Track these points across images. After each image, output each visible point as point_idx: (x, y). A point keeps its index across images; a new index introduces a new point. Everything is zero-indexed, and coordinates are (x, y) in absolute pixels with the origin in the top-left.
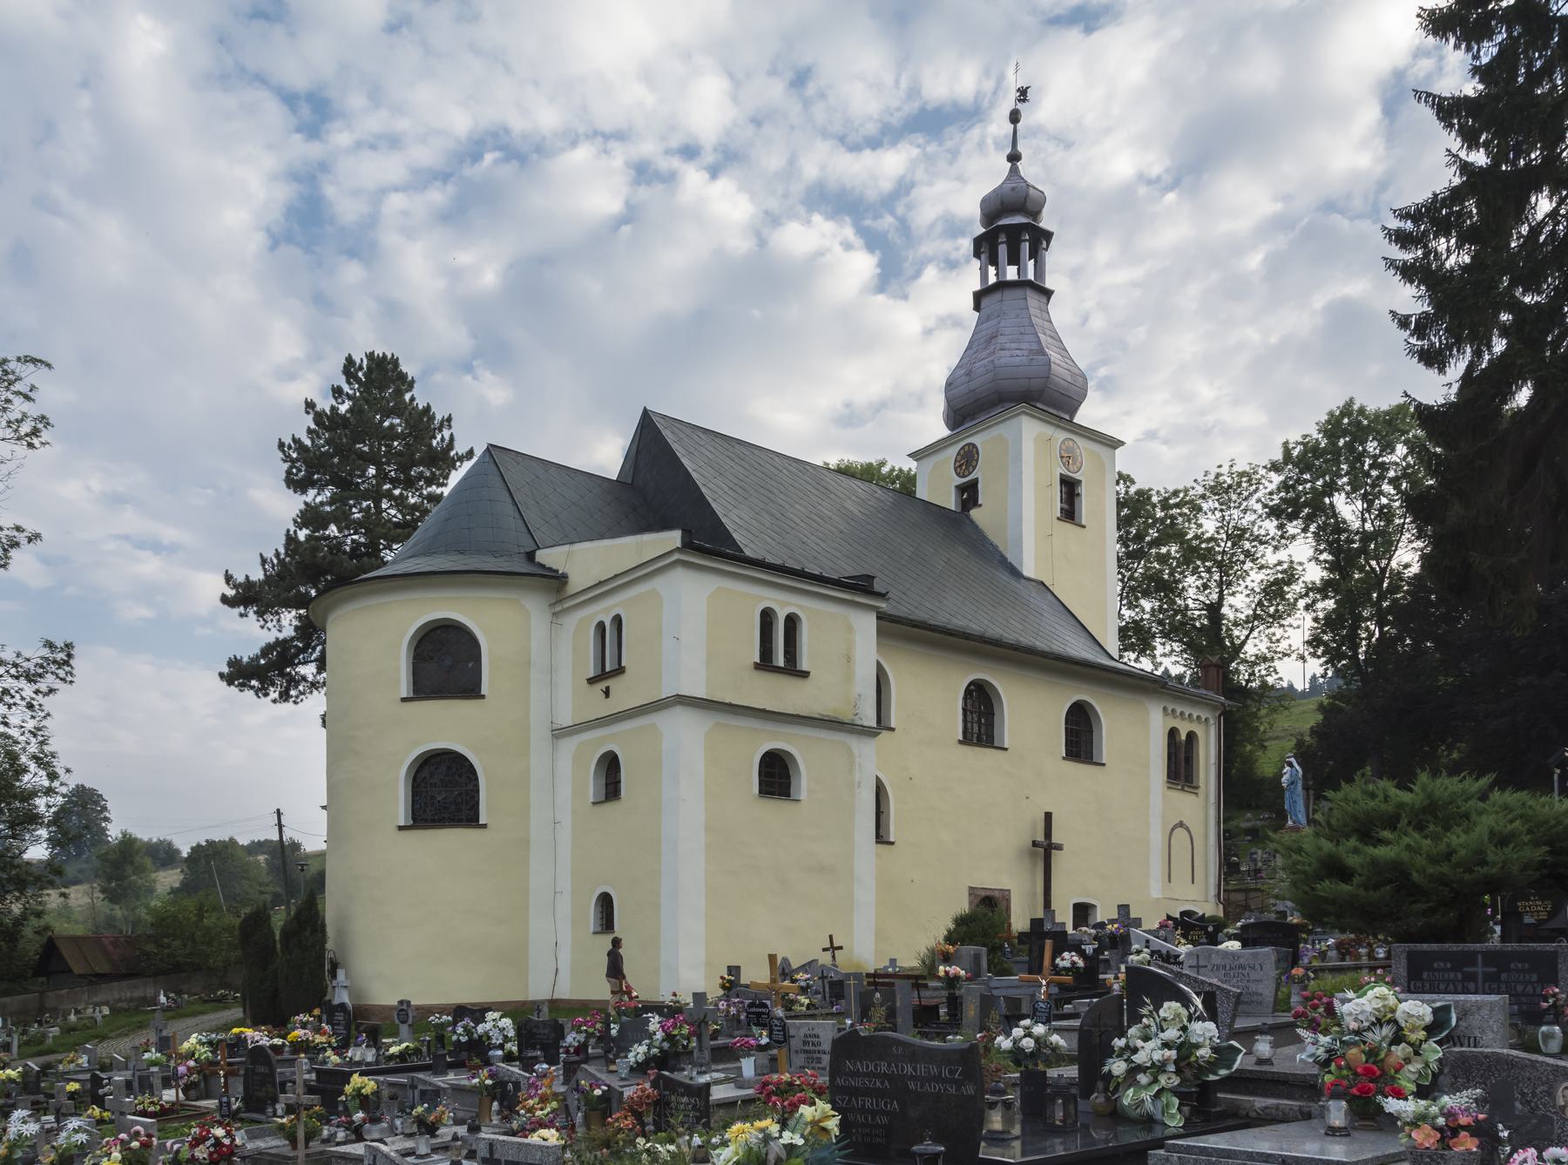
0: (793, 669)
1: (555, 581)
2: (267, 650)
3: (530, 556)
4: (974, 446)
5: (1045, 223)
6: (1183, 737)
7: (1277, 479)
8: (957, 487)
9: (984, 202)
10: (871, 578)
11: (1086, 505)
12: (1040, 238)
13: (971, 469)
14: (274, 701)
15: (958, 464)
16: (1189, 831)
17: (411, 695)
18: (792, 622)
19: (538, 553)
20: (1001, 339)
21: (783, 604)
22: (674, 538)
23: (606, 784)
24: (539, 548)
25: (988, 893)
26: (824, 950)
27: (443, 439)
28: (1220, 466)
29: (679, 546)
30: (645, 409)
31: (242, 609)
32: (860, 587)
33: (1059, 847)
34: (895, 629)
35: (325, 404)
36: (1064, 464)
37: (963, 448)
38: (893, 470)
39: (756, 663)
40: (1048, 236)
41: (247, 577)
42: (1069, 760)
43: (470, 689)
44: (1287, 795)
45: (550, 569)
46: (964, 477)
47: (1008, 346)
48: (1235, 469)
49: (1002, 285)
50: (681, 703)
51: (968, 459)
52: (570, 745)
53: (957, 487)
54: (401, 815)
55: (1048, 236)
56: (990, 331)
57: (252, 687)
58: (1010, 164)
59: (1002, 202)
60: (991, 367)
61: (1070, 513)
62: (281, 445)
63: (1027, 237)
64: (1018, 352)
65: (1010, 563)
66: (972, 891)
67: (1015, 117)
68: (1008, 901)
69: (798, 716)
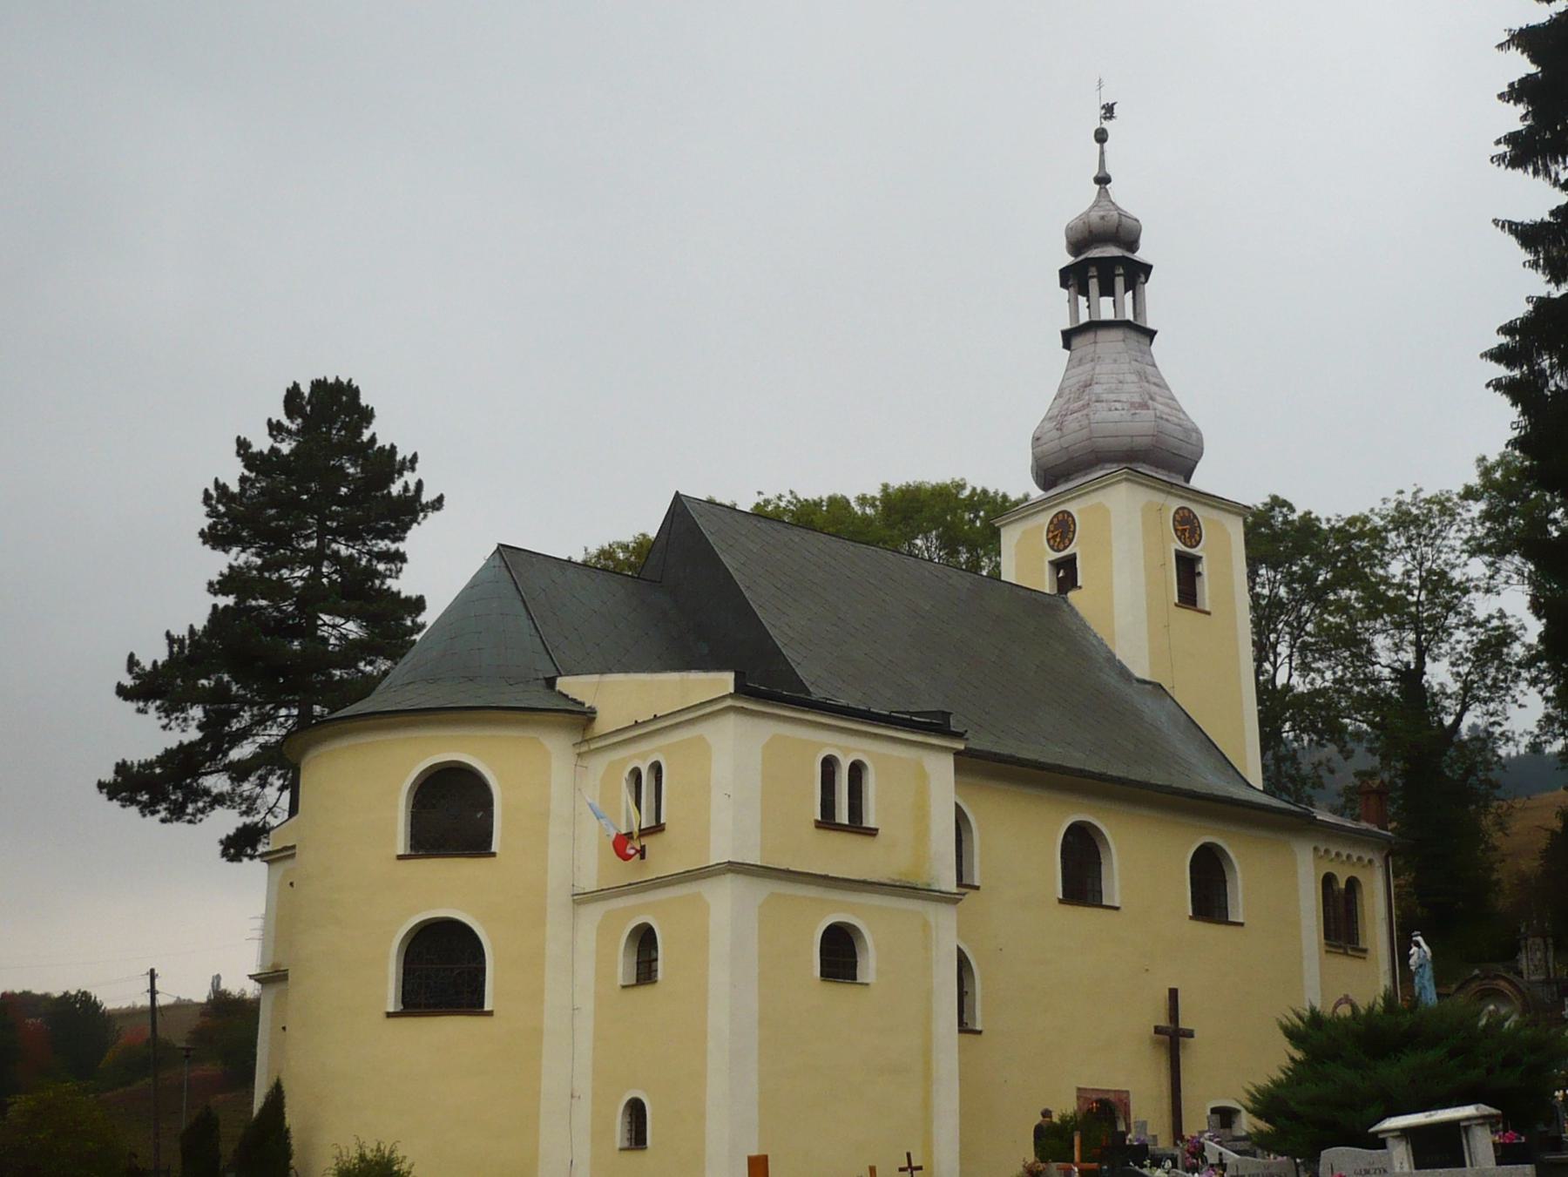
0: (856, 825)
1: (580, 718)
2: (168, 757)
3: (550, 682)
4: (1069, 514)
5: (1141, 255)
6: (1342, 885)
7: (1477, 508)
8: (1051, 563)
9: (1069, 230)
10: (946, 715)
11: (1206, 589)
12: (1138, 273)
13: (1067, 541)
14: (163, 821)
15: (1051, 535)
17: (634, 981)
18: (857, 770)
19: (559, 680)
20: (1097, 389)
21: (847, 747)
22: (725, 681)
23: (638, 963)
24: (561, 675)
26: (901, 1170)
27: (406, 488)
28: (1401, 492)
29: (732, 691)
30: (677, 492)
31: (141, 704)
32: (935, 725)
33: (1190, 1034)
34: (972, 765)
35: (262, 443)
36: (1180, 538)
38: (974, 489)
39: (817, 821)
40: (1146, 269)
42: (1197, 919)
43: (476, 843)
44: (1417, 979)
45: (574, 700)
46: (1059, 550)
47: (1105, 396)
48: (1422, 495)
49: (1095, 326)
50: (730, 871)
51: (1062, 530)
52: (595, 912)
53: (1051, 563)
54: (391, 999)
55: (1146, 269)
56: (1083, 378)
57: (139, 803)
58: (1098, 187)
59: (1090, 232)
60: (1085, 422)
61: (1188, 596)
63: (1121, 271)
64: (1118, 405)
65: (1119, 662)
67: (1101, 136)
68: (1127, 1105)
69: (864, 882)
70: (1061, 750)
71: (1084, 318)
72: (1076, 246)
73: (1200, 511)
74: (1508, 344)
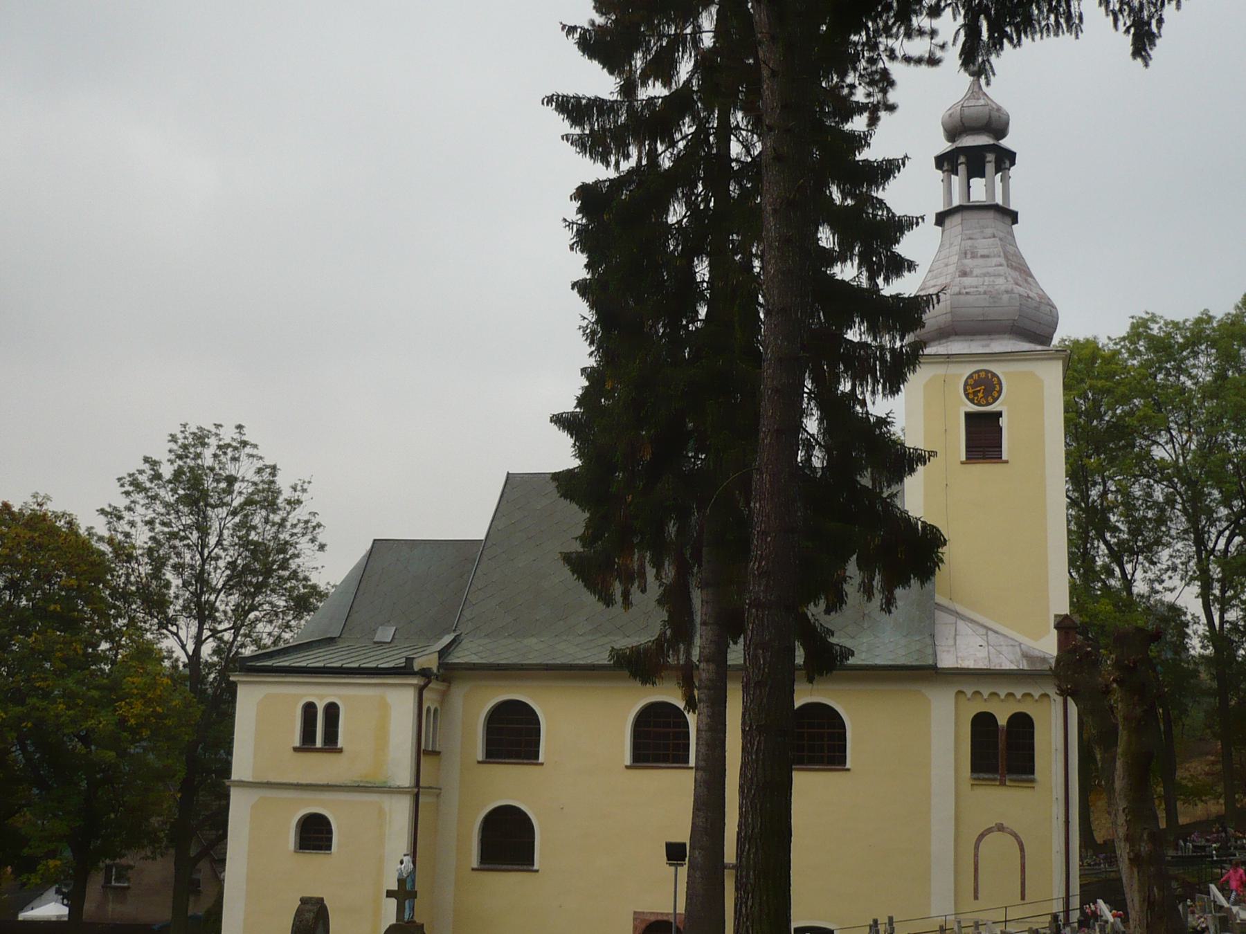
5: (1005, 143)
16: (1016, 836)
18: (332, 711)
21: (321, 694)
25: (660, 918)
36: (972, 401)
37: (977, 372)
41: (561, 421)
46: (979, 404)
53: (969, 416)
62: (1077, 37)
66: (635, 913)
70: (71, 730)
71: (956, 202)
72: (953, 133)
73: (997, 368)
74: (887, 280)
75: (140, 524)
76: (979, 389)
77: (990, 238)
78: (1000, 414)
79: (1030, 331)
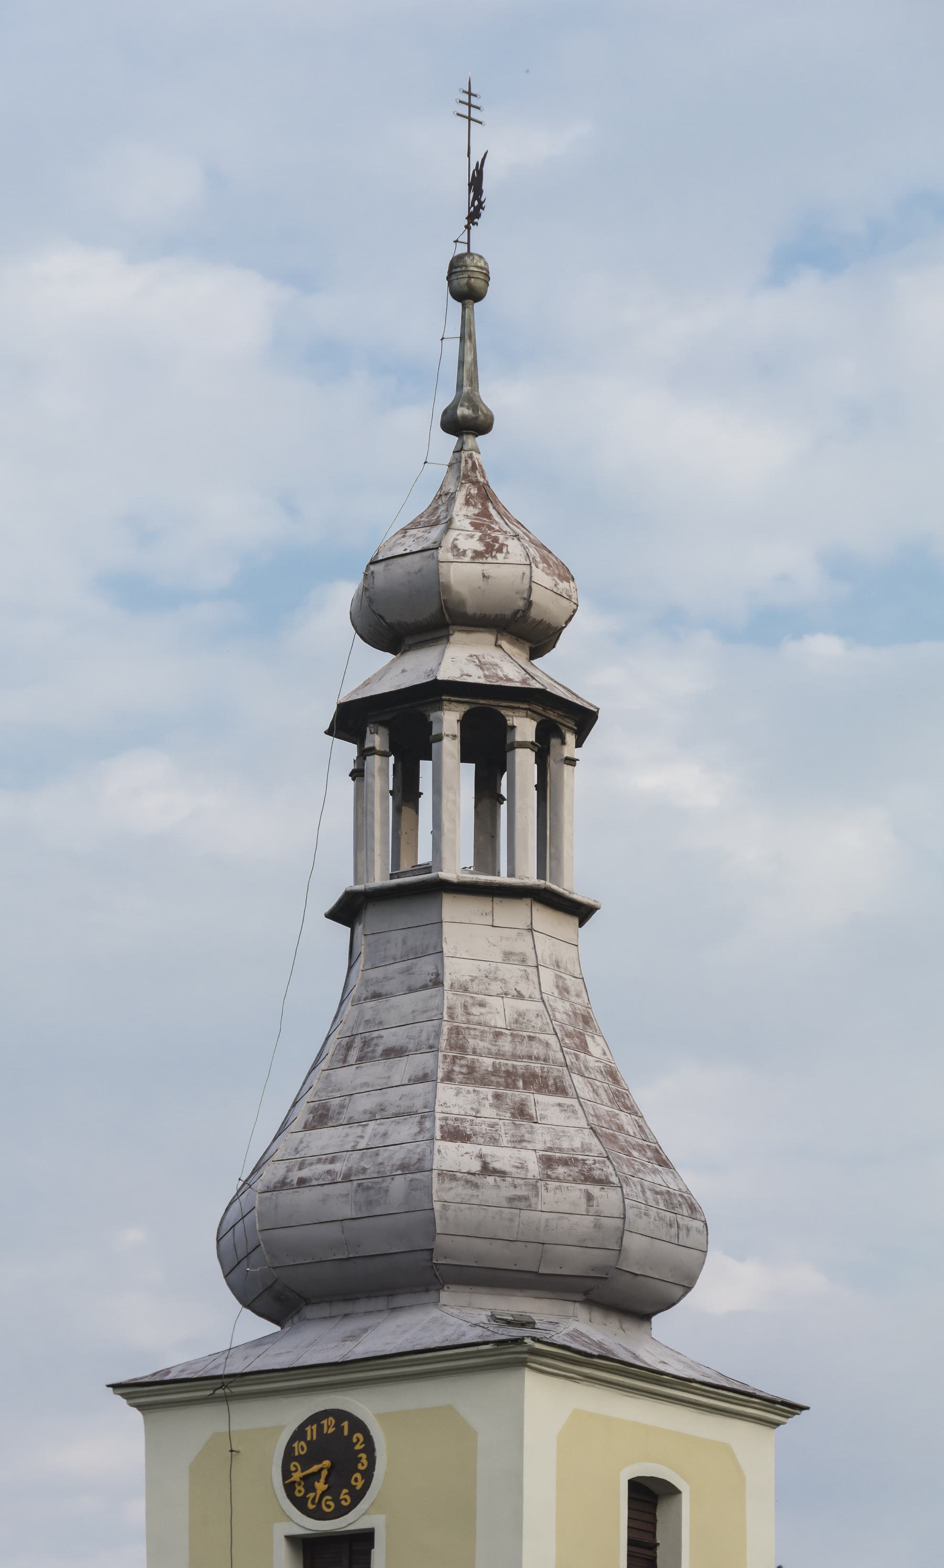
37: (316, 1419)
41: (422, 794)
46: (318, 1514)
75: (573, 993)
76: (315, 1468)
77: (425, 987)
78: (366, 1538)
79: (376, 1297)
